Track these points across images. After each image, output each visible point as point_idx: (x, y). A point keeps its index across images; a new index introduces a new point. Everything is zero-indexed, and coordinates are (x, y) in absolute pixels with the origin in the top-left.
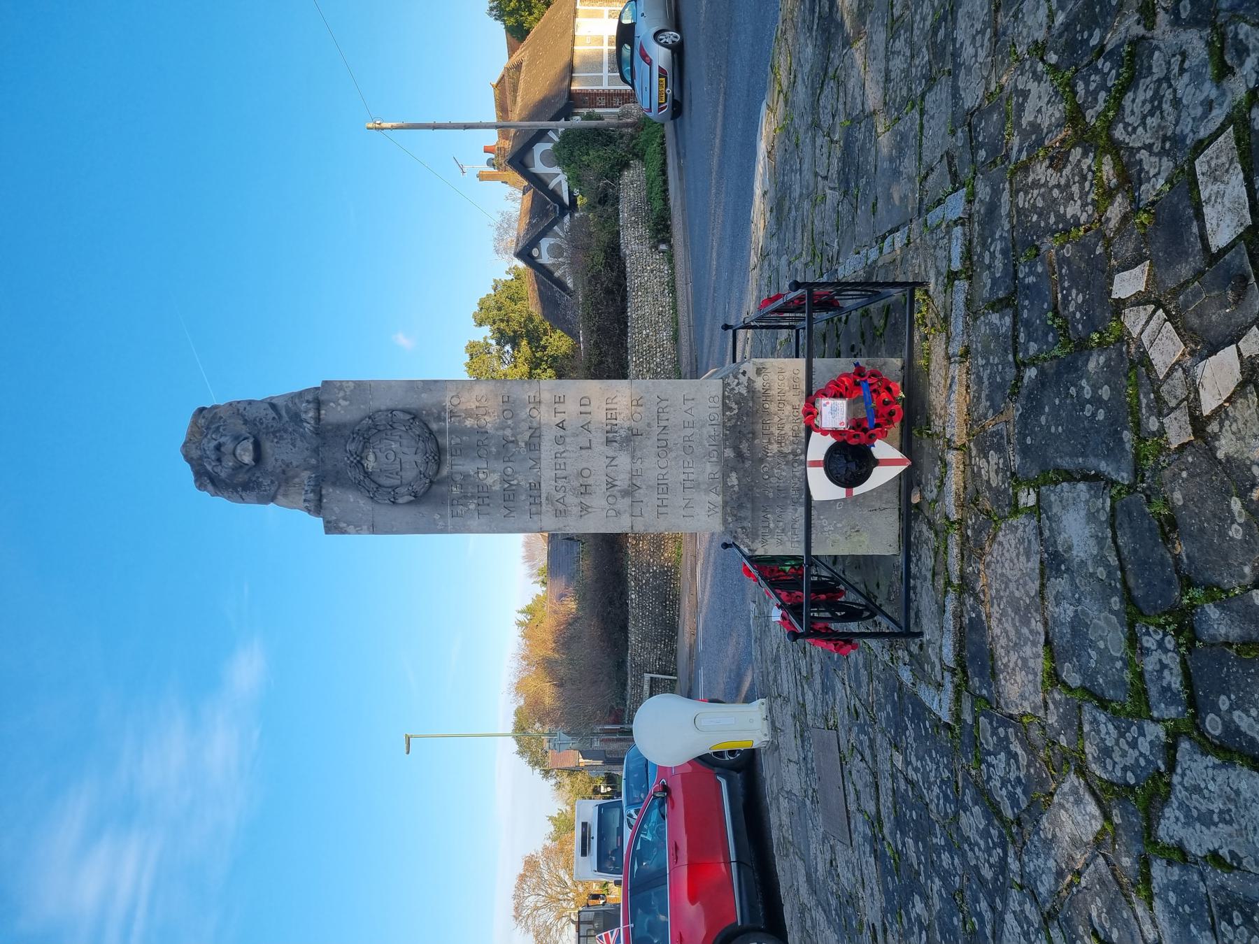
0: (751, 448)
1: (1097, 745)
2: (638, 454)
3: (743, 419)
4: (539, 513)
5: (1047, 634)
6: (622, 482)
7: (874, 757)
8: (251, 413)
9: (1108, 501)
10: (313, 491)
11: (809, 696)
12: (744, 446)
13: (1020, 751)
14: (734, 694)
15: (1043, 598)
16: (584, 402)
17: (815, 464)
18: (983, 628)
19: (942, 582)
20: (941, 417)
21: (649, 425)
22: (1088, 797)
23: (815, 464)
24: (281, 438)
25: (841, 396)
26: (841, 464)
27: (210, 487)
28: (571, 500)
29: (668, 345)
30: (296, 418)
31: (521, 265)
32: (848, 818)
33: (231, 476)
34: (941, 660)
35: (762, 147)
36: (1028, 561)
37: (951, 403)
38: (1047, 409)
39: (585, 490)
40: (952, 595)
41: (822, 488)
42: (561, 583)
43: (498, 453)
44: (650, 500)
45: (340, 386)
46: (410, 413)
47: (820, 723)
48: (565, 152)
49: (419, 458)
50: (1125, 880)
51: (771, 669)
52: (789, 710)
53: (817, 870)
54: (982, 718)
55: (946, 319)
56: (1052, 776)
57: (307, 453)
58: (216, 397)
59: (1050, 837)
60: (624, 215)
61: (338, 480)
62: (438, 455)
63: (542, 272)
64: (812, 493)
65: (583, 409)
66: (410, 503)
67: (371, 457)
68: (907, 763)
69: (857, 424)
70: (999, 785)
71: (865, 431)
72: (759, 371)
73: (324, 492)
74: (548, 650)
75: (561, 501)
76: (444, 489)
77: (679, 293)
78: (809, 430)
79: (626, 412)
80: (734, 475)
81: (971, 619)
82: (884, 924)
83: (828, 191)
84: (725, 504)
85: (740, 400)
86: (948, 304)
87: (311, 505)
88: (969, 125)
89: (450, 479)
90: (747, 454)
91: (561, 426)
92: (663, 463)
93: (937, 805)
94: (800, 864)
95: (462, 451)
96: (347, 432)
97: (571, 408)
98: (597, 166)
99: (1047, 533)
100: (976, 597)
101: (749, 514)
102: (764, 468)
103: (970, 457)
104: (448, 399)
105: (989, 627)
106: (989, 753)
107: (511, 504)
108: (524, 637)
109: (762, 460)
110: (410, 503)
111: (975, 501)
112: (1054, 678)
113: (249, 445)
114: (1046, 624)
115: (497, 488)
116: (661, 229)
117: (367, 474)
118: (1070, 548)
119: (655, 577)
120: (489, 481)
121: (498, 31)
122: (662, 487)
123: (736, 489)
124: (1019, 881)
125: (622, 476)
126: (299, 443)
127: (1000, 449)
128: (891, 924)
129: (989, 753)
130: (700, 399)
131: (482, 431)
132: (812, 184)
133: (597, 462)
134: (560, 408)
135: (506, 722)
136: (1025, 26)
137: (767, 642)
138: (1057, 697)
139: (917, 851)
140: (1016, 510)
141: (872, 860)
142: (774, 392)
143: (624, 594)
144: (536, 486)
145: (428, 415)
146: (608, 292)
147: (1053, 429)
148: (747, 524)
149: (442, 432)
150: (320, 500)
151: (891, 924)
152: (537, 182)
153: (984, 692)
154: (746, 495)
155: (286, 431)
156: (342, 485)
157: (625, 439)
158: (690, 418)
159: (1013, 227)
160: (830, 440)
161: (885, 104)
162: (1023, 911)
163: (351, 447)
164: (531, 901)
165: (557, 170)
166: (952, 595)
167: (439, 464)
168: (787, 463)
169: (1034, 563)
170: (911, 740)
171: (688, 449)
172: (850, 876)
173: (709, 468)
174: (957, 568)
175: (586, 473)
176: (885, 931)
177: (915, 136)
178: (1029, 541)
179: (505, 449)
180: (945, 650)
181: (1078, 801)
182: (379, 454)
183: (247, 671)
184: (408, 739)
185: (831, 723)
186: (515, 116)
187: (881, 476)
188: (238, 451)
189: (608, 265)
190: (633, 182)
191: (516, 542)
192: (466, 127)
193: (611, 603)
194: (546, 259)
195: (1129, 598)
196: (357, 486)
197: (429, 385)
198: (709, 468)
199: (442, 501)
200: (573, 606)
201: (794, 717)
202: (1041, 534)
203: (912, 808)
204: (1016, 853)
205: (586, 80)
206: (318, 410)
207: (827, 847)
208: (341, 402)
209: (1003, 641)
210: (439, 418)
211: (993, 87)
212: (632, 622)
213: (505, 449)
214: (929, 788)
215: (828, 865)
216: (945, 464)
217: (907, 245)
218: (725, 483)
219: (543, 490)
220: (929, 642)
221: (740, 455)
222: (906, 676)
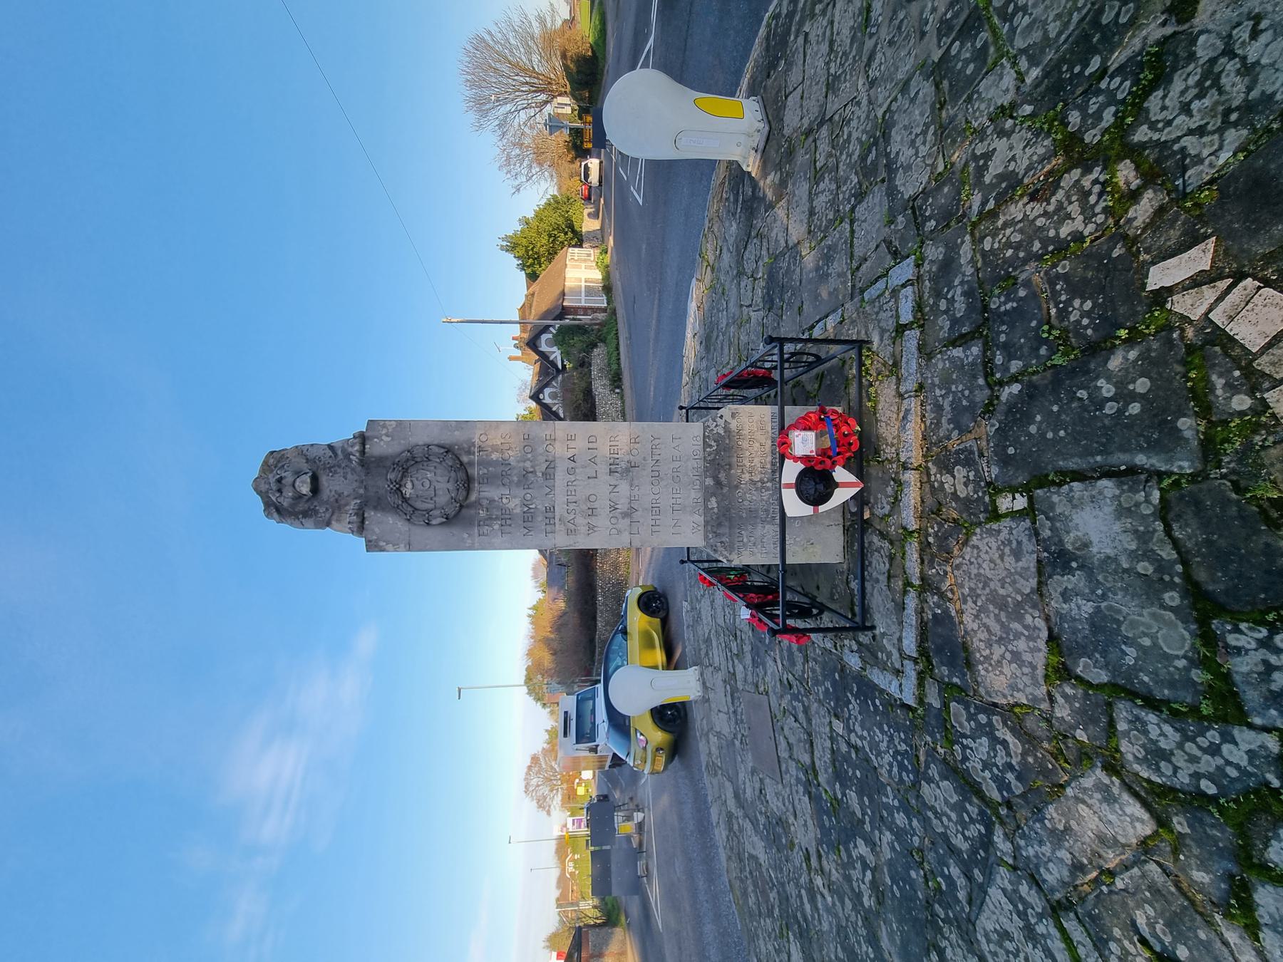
0: (728, 476)
1: (1143, 746)
2: (636, 482)
3: (720, 457)
4: (553, 532)
5: (1050, 630)
6: (623, 506)
7: (809, 721)
8: (313, 453)
9: (1156, 495)
10: (356, 514)
11: (739, 668)
12: (722, 476)
13: (1009, 738)
15: (1041, 595)
16: (591, 439)
17: (788, 486)
18: (953, 624)
19: (900, 583)
20: (893, 445)
21: (644, 459)
22: (1126, 797)
23: (788, 486)
24: (335, 472)
25: (810, 429)
26: (810, 487)
27: (275, 515)
28: (581, 521)
30: (347, 456)
31: (533, 404)
33: (293, 506)
34: (900, 650)
35: (692, 306)
36: (1018, 560)
37: (903, 429)
38: (1038, 418)
39: (592, 512)
40: (912, 594)
41: (794, 506)
43: (519, 481)
45: (384, 424)
46: (443, 447)
47: (750, 688)
48: (560, 338)
49: (451, 486)
50: (1199, 897)
51: (703, 646)
52: (719, 676)
54: (953, 704)
55: (896, 364)
56: (1063, 768)
57: (355, 485)
58: (287, 442)
59: (1061, 828)
60: (594, 373)
61: (379, 505)
62: (468, 483)
64: (786, 511)
65: (591, 445)
67: (409, 485)
68: (850, 731)
69: (823, 453)
70: (979, 767)
71: (830, 457)
72: (733, 415)
74: (547, 632)
75: (572, 522)
76: (472, 512)
78: (782, 458)
79: (626, 448)
80: (713, 499)
81: (935, 615)
83: (752, 314)
84: (706, 523)
85: (718, 439)
86: (897, 353)
87: (355, 527)
88: (913, 208)
89: (478, 504)
90: (725, 482)
91: (572, 459)
92: (656, 490)
93: (890, 772)
94: (728, 784)
95: (488, 480)
96: (388, 463)
97: (580, 444)
98: (579, 345)
99: (1046, 533)
100: (942, 595)
102: (739, 493)
103: (929, 475)
104: (477, 436)
105: (961, 622)
106: (964, 736)
107: (529, 524)
108: (532, 623)
109: (737, 487)
110: (441, 524)
111: (938, 512)
112: (1062, 672)
113: (307, 478)
114: (1047, 619)
115: (518, 510)
116: (616, 381)
117: (405, 500)
118: (1086, 545)
120: (511, 505)
121: (522, 276)
124: (1010, 861)
125: (622, 501)
126: (349, 476)
127: (969, 463)
128: (827, 854)
129: (964, 736)
131: (505, 463)
132: (737, 313)
133: (602, 489)
134: (572, 444)
135: (520, 676)
136: (982, 100)
137: (699, 628)
138: (1069, 691)
139: (861, 803)
140: (995, 515)
141: (806, 799)
143: (594, 597)
144: (551, 510)
147: (1050, 435)
149: (471, 464)
150: (363, 522)
151: (827, 854)
152: (543, 356)
153: (955, 680)
155: (339, 466)
156: (383, 510)
157: (624, 470)
159: (978, 270)
160: (800, 466)
161: (809, 232)
162: (1016, 891)
163: (391, 476)
164: (534, 782)
165: (555, 349)
166: (912, 594)
167: (468, 490)
168: (757, 489)
169: (1029, 562)
170: (855, 713)
172: (780, 804)
173: (693, 494)
174: (917, 570)
176: (820, 857)
177: (845, 242)
178: (1019, 543)
179: (525, 478)
180: (905, 642)
181: (1109, 799)
182: (416, 482)
183: (366, 642)
185: (761, 689)
186: (533, 318)
187: (841, 496)
188: (297, 484)
190: (599, 356)
191: (530, 557)
192: (501, 322)
193: (586, 602)
194: (548, 400)
195: (1193, 590)
196: (396, 509)
198: (693, 494)
199: (470, 523)
200: (563, 605)
201: (725, 681)
202: (1037, 534)
203: (855, 767)
204: (1006, 834)
205: (572, 300)
206: (363, 444)
207: (756, 778)
208: (384, 438)
209: (983, 635)
210: (469, 453)
211: (940, 168)
212: (599, 614)
213: (525, 478)
214: (879, 754)
215: (757, 792)
216: (899, 483)
217: (841, 323)
218: (706, 507)
219: (557, 514)
220: (883, 634)
221: (718, 483)
222: (854, 662)
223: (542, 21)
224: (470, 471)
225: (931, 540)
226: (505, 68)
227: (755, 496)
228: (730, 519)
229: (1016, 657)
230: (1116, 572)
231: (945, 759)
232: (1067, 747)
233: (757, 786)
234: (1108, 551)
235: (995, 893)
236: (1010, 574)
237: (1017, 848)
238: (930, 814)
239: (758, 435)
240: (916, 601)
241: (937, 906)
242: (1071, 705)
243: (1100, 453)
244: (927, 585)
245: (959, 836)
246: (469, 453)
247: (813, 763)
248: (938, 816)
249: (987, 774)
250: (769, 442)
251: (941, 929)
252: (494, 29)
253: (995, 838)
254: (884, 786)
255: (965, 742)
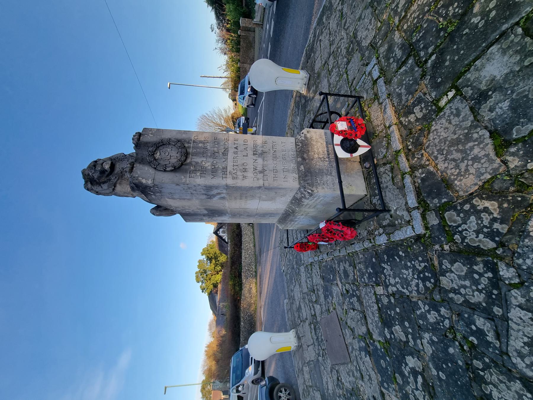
2: (265, 159)
3: (303, 150)
6: (260, 168)
12: (305, 156)
14: (283, 328)
15: (478, 121)
17: (337, 145)
21: (269, 150)
23: (337, 145)
28: (239, 173)
29: (252, 248)
32: (347, 348)
33: (99, 178)
37: (383, 116)
39: (245, 170)
41: (341, 154)
42: (219, 327)
43: (211, 156)
44: (271, 175)
53: (328, 389)
62: (187, 155)
63: (220, 238)
65: (245, 143)
66: (172, 171)
67: (158, 154)
72: (308, 132)
73: (135, 166)
76: (187, 167)
77: (255, 235)
82: (382, 392)
84: (299, 177)
85: (302, 142)
89: (190, 164)
91: (236, 148)
92: (275, 162)
95: (196, 154)
101: (310, 177)
109: (312, 160)
110: (172, 171)
115: (209, 168)
117: (155, 159)
119: (249, 317)
120: (206, 165)
122: (275, 171)
123: (304, 170)
125: (259, 166)
129: (459, 226)
130: (287, 144)
133: (250, 161)
134: (236, 142)
142: (314, 138)
143: (239, 324)
145: (184, 141)
146: (237, 235)
148: (309, 182)
149: (189, 147)
154: (308, 171)
156: (144, 164)
158: (283, 148)
160: (341, 138)
168: (322, 161)
171: (284, 159)
173: (292, 165)
175: (245, 164)
182: (162, 153)
183: (124, 360)
184: (166, 388)
189: (237, 229)
193: (235, 327)
194: (221, 234)
196: (149, 163)
197: (185, 132)
199: (186, 171)
213: (214, 155)
218: (298, 170)
221: (304, 159)
223: (226, 111)
224: (188, 150)
225: (410, 147)
226: (211, 124)
227: (321, 164)
228: (311, 173)
229: (476, 159)
230: (514, 76)
231: (450, 251)
232: (526, 178)
233: (335, 377)
234: (505, 72)
235: (515, 314)
236: (456, 125)
237: (518, 267)
238: (451, 295)
239: (320, 140)
240: (410, 178)
241: (475, 361)
242: (517, 156)
243: (484, 42)
244: (413, 168)
245: (476, 293)
246: (189, 143)
247: (368, 330)
248: (456, 291)
249: (481, 236)
250: (325, 143)
251: (483, 377)
252: (209, 113)
253: (501, 273)
254: (416, 303)
255: (460, 229)
